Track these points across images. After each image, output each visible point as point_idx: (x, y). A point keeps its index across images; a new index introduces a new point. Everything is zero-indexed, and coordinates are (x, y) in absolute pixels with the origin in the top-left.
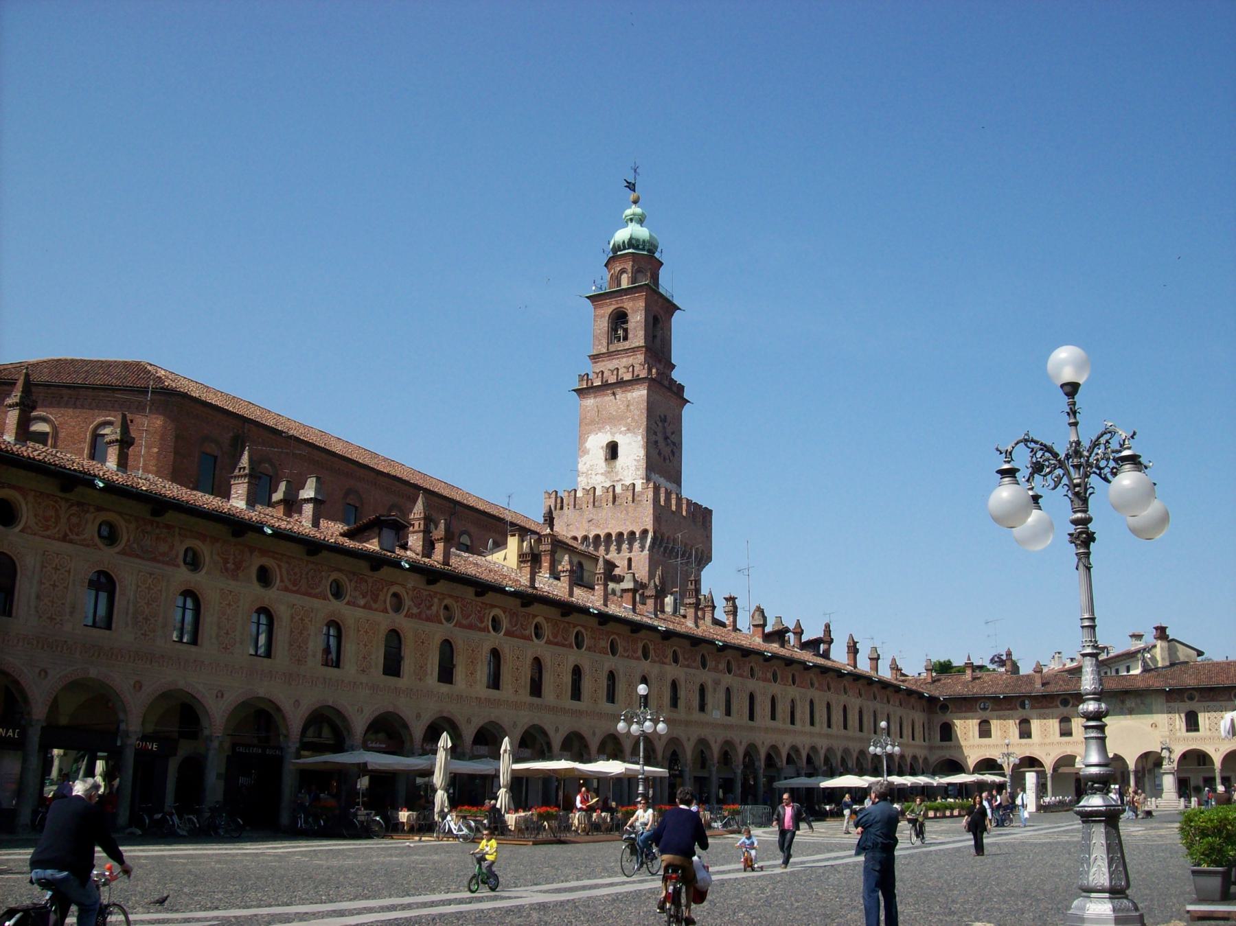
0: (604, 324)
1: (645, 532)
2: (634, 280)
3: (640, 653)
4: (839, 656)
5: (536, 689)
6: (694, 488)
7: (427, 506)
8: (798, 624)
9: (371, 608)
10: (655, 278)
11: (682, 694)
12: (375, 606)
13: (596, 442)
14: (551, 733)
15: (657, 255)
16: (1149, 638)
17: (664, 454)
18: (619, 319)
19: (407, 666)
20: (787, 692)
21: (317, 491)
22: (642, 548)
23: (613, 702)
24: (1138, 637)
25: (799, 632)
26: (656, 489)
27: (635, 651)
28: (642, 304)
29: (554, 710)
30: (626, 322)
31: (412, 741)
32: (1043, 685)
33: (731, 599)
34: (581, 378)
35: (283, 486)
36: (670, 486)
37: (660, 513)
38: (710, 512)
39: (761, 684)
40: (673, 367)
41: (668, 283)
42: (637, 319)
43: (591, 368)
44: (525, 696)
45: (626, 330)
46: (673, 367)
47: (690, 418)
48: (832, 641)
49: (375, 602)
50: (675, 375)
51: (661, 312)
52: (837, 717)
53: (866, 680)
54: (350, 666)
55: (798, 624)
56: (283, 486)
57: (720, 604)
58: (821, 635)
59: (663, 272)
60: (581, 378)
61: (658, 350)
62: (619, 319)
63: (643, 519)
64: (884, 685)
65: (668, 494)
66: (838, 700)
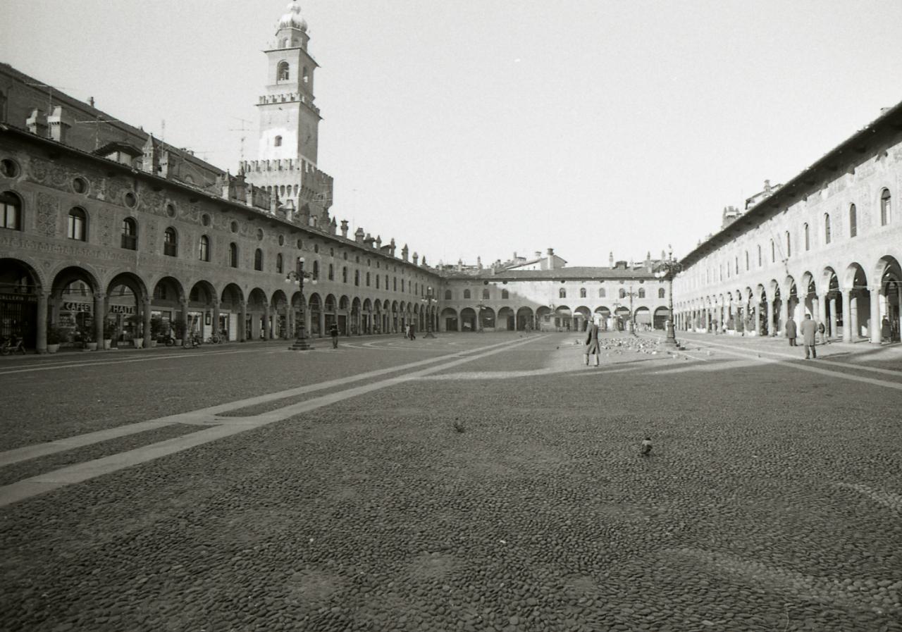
0: (274, 70)
1: (297, 186)
2: (293, 45)
3: (296, 245)
4: (398, 254)
5: (258, 266)
6: (324, 165)
7: (170, 158)
8: (379, 238)
9: (109, 202)
10: (305, 45)
11: (320, 269)
12: (113, 201)
13: (271, 134)
14: (243, 288)
15: (307, 33)
16: (545, 255)
17: (308, 144)
18: (284, 67)
19: (141, 242)
20: (373, 269)
21: (62, 116)
22: (296, 194)
23: (260, 270)
24: (539, 253)
25: (379, 241)
26: (304, 162)
27: (293, 243)
28: (297, 59)
29: (244, 275)
30: (287, 69)
31: (146, 291)
32: (496, 273)
33: (345, 222)
34: (261, 98)
35: (35, 113)
36: (311, 163)
37: (305, 177)
38: (332, 179)
39: (351, 263)
40: (314, 98)
41: (312, 50)
42: (294, 69)
43: (266, 93)
44: (253, 271)
45: (287, 74)
46: (314, 98)
47: (324, 130)
48: (395, 247)
49: (114, 198)
50: (315, 102)
51: (308, 65)
52: (391, 284)
53: (408, 266)
54: (242, 266)
55: (379, 238)
56: (35, 113)
57: (339, 224)
58: (390, 244)
59: (310, 44)
60: (261, 98)
61: (306, 89)
62: (284, 67)
63: (295, 179)
64: (419, 268)
65: (310, 166)
66: (400, 276)
